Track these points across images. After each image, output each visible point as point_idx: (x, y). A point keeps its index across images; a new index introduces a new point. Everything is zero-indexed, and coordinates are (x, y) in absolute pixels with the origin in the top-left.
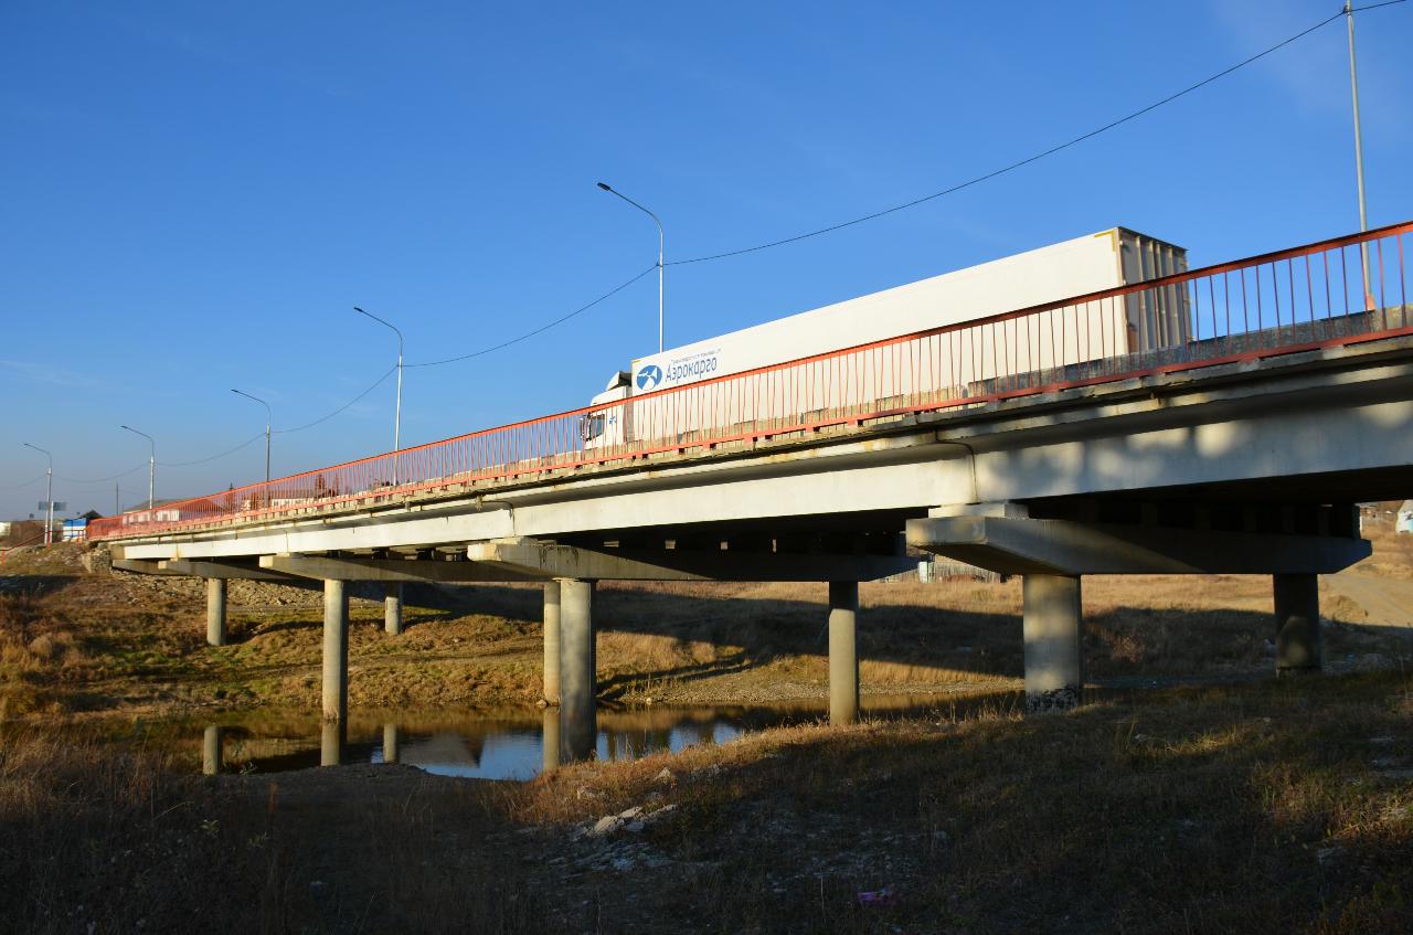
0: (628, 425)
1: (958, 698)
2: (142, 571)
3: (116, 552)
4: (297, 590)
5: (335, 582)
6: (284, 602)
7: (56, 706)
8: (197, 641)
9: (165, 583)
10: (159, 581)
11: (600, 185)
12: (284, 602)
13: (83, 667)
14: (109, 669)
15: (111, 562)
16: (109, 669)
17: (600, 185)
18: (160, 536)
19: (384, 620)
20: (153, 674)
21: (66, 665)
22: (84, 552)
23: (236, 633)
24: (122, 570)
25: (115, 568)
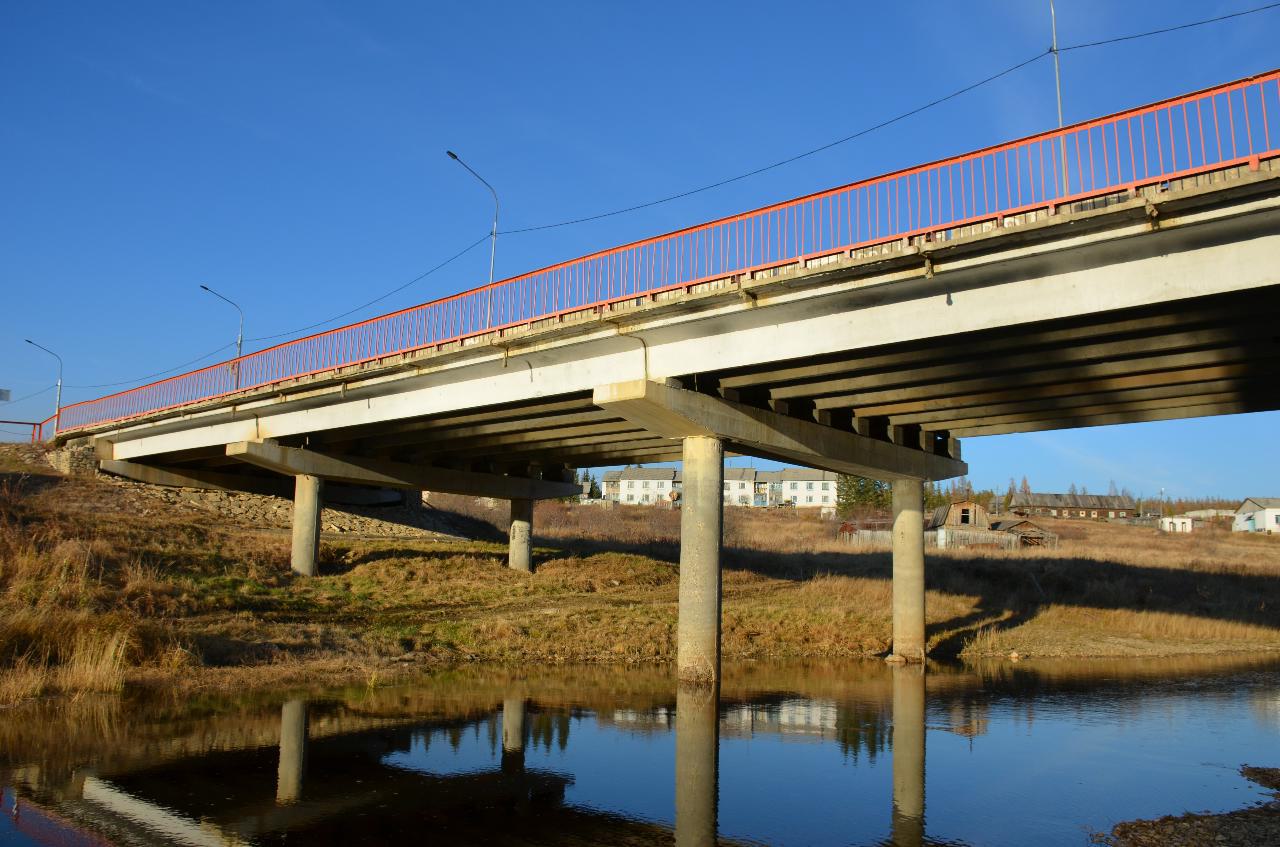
0: (1216, 200)
1: (319, 701)
2: (139, 478)
3: (103, 450)
4: (347, 515)
5: (711, 441)
6: (342, 530)
7: (178, 654)
8: (279, 567)
9: (178, 494)
10: (170, 491)
11: (449, 153)
12: (342, 530)
13: (157, 594)
14: (198, 598)
15: (98, 463)
16: (198, 598)
17: (449, 153)
18: (235, 403)
19: (508, 555)
20: (1213, 508)
21: (129, 587)
22: (48, 451)
23: (329, 562)
24: (113, 475)
25: (103, 472)
